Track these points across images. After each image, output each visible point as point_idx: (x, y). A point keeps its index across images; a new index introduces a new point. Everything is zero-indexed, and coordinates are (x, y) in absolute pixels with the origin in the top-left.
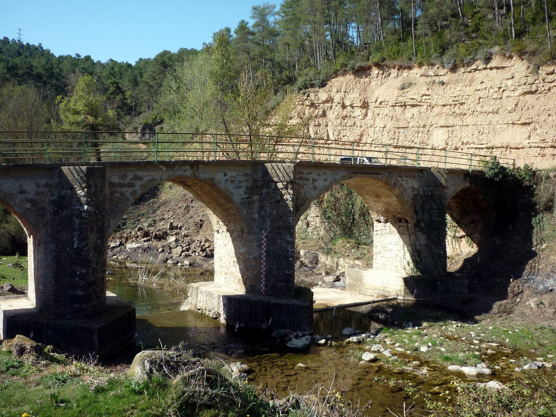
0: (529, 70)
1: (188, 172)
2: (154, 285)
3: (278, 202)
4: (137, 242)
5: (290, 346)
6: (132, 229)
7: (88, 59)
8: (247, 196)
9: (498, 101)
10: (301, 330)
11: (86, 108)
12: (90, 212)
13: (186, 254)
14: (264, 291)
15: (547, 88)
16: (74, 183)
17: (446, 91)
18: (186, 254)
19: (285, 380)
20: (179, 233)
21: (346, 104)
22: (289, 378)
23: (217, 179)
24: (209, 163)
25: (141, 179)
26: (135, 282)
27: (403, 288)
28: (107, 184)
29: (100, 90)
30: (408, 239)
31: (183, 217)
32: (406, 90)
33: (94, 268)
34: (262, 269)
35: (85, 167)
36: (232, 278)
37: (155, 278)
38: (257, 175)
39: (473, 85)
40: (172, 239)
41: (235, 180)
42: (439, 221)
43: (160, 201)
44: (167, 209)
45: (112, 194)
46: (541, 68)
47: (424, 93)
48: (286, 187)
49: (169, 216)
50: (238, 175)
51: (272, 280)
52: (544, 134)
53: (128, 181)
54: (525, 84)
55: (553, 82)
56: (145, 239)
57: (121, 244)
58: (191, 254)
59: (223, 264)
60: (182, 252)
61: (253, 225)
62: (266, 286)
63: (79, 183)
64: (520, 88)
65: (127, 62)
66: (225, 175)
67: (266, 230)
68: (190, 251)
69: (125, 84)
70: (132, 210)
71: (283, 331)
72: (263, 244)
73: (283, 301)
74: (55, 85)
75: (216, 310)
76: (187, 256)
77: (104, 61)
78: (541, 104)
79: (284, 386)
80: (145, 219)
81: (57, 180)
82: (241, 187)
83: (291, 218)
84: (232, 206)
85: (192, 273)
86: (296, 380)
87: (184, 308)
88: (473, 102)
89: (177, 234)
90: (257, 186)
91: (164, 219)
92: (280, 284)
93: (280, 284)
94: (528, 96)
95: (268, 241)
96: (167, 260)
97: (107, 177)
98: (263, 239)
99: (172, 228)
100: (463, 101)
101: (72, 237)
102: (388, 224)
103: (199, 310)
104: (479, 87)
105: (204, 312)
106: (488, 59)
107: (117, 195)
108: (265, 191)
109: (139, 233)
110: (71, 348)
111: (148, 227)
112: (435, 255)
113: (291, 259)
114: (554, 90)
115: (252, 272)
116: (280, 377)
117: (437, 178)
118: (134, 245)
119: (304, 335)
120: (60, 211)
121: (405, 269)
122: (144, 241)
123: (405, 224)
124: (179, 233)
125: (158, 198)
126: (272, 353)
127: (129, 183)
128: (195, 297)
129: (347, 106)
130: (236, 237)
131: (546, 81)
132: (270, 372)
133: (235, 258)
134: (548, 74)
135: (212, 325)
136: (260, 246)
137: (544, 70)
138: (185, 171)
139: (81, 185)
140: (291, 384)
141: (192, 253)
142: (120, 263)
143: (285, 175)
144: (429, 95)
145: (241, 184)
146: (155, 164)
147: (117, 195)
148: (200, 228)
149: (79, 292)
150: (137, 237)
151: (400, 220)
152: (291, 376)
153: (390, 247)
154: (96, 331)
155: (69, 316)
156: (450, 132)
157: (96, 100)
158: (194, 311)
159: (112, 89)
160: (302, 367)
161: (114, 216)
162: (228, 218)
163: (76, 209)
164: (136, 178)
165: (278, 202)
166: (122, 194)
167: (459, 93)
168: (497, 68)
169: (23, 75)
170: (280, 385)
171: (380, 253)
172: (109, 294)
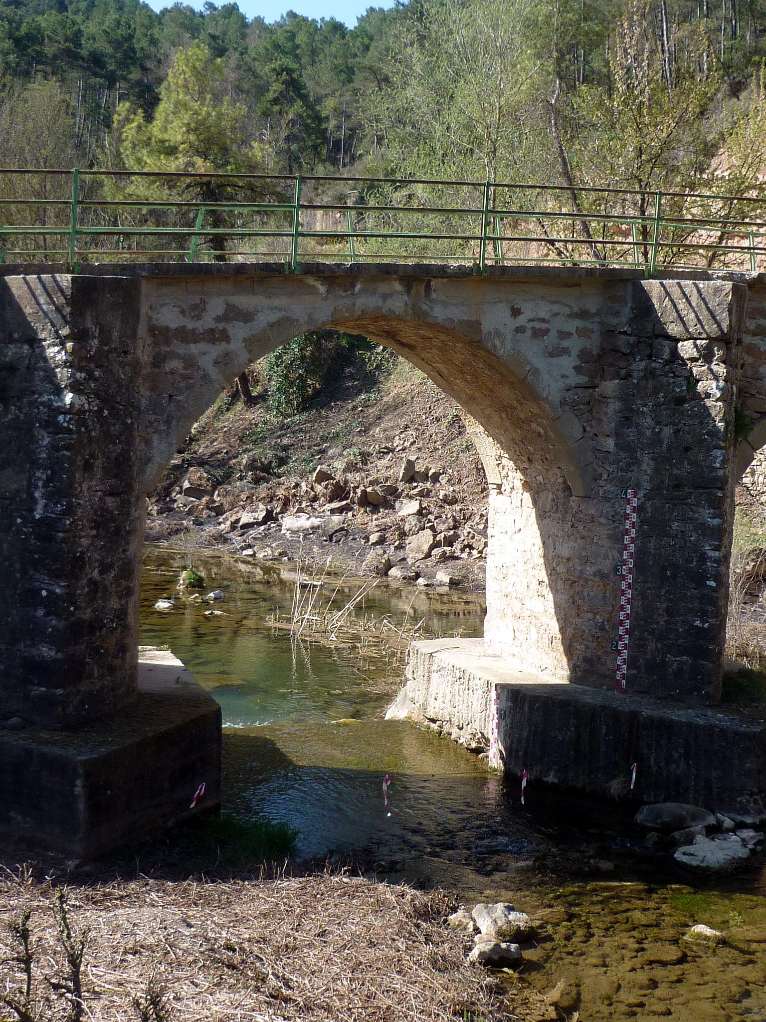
1: (396, 300)
2: (333, 637)
3: (680, 401)
5: (685, 859)
6: (303, 475)
7: (230, 14)
8: (583, 379)
10: (729, 808)
11: (192, 137)
12: (81, 412)
13: (444, 552)
16: (37, 326)
18: (444, 552)
19: (642, 977)
20: (429, 491)
22: (659, 973)
23: (487, 326)
24: (462, 274)
25: (247, 317)
26: (284, 625)
28: (142, 330)
29: (247, 92)
31: (444, 445)
33: (92, 582)
35: (69, 276)
36: (533, 631)
37: (338, 618)
38: (618, 321)
40: (408, 508)
41: (547, 331)
43: (385, 399)
44: (402, 422)
45: (158, 361)
48: (706, 356)
49: (407, 444)
51: (651, 646)
53: (207, 322)
56: (336, 505)
57: (270, 517)
58: (458, 554)
59: (510, 589)
60: (432, 547)
62: (631, 663)
63: (53, 325)
65: (332, 19)
66: (516, 312)
67: (637, 487)
68: (457, 546)
69: (319, 78)
70: (307, 422)
71: (670, 808)
72: (627, 532)
73: (679, 715)
74: (139, 83)
75: (477, 725)
76: (446, 558)
77: (271, 18)
79: (632, 1000)
80: (338, 451)
82: (565, 351)
83: (718, 453)
84: (535, 410)
85: (461, 607)
86: (679, 981)
87: (395, 712)
90: (615, 350)
91: (393, 451)
92: (674, 661)
93: (674, 661)
95: (642, 522)
96: (389, 566)
97: (144, 309)
98: (626, 516)
99: (411, 476)
103: (434, 721)
105: (445, 729)
107: (174, 364)
109: (319, 488)
111: (345, 471)
113: (713, 584)
115: (590, 616)
116: (628, 965)
118: (304, 522)
119: (741, 826)
122: (333, 511)
124: (429, 491)
126: (621, 881)
127: (212, 331)
128: (423, 684)
132: (601, 944)
133: (544, 573)
135: (463, 770)
136: (617, 538)
138: (385, 297)
139: (56, 332)
140: (658, 992)
141: (462, 550)
142: (267, 570)
143: (704, 315)
145: (565, 344)
146: (292, 272)
147: (174, 364)
149: (46, 652)
150: (315, 499)
152: (664, 964)
154: (80, 771)
155: (15, 720)
157: (220, 116)
159: (276, 88)
160: (707, 938)
161: (163, 428)
162: (524, 448)
164: (233, 314)
165: (680, 401)
166: (190, 362)
169: (55, 57)
170: (623, 995)
172: (159, 657)
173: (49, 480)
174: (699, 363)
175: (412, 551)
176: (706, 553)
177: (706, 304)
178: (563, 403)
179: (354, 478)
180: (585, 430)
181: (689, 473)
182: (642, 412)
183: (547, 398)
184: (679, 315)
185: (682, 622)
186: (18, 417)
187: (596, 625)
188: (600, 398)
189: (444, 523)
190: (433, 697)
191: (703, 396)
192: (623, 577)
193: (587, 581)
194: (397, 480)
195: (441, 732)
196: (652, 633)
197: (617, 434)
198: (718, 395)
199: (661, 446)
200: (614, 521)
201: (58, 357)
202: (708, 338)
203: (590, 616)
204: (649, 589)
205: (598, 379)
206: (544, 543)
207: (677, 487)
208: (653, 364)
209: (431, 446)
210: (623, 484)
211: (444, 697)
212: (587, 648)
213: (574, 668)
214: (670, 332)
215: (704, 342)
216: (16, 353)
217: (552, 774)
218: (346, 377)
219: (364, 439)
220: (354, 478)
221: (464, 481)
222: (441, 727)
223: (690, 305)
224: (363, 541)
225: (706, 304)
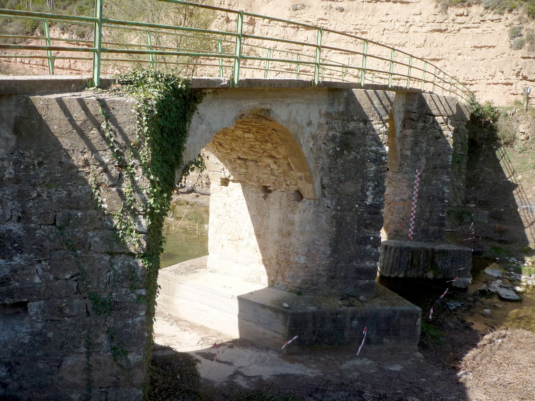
3: (437, 138)
9: (404, 35)
14: (412, 236)
17: (345, 18)
21: (231, 19)
32: (298, 11)
34: (412, 211)
39: (377, 15)
46: (449, 8)
47: (321, 17)
51: (423, 224)
52: (455, 71)
55: (463, 23)
61: (403, 162)
63: (379, 114)
64: (428, 25)
67: (419, 168)
81: (341, 108)
88: (377, 32)
92: (432, 229)
95: (421, 181)
98: (416, 179)
100: (365, 30)
101: (363, 190)
104: (384, 19)
108: (420, 124)
110: (385, 340)
112: (455, 187)
115: (397, 215)
117: (463, 113)
120: (345, 152)
129: (231, 21)
131: (456, 21)
134: (457, 16)
136: (411, 187)
139: (381, 118)
143: (447, 108)
144: (326, 20)
156: (351, 60)
163: (372, 151)
165: (437, 138)
167: (361, 21)
173: (376, 186)
177: (448, 104)
184: (437, 107)
186: (356, 157)
187: (400, 218)
193: (396, 203)
196: (424, 219)
201: (382, 129)
202: (448, 116)
207: (435, 168)
210: (414, 168)
212: (396, 226)
216: (355, 127)
217: (402, 274)
225: (448, 104)
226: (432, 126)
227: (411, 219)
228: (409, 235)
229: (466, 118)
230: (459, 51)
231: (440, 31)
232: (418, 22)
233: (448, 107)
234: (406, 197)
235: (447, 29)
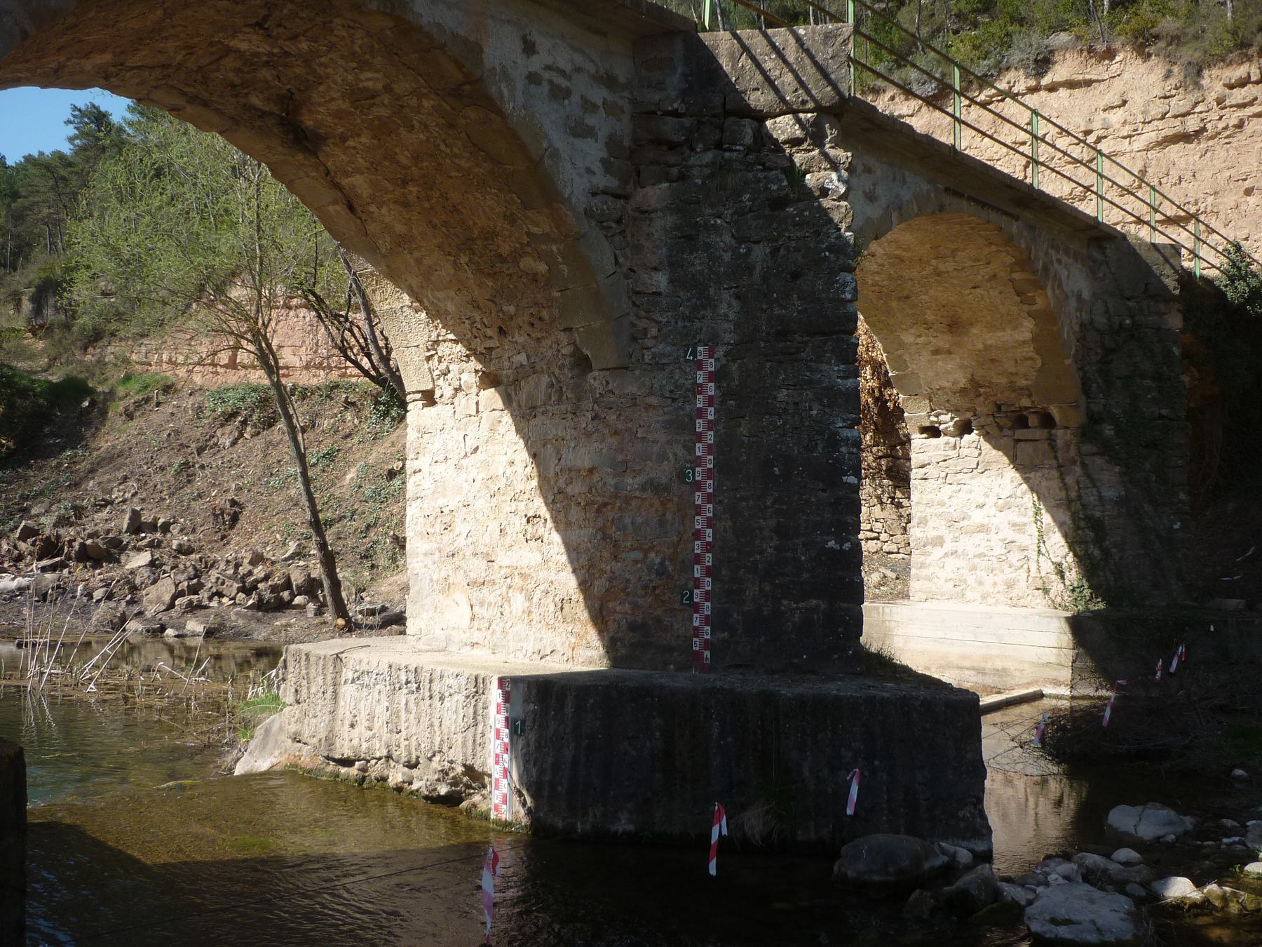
0: (1173, 81)
4: (19, 573)
8: (613, 183)
13: (191, 602)
14: (707, 645)
15: (1234, 121)
18: (191, 602)
20: (160, 542)
27: (1068, 655)
30: (1056, 484)
31: (171, 495)
34: (698, 535)
36: (519, 602)
42: (1161, 417)
44: (120, 475)
46: (1206, 73)
49: (128, 495)
50: (578, 70)
54: (1163, 118)
55: (1251, 103)
56: (45, 562)
58: (205, 602)
59: (461, 542)
60: (174, 597)
61: (642, 324)
64: (1147, 128)
67: (712, 342)
68: (204, 594)
76: (193, 608)
78: (1218, 164)
82: (589, 132)
89: (152, 545)
91: (111, 503)
94: (1174, 150)
95: (726, 395)
96: (123, 619)
98: (697, 389)
99: (137, 527)
102: (974, 436)
103: (347, 762)
106: (1043, 63)
109: (23, 546)
111: (56, 525)
114: (1254, 126)
115: (638, 555)
121: (1046, 591)
122: (44, 569)
123: (1041, 434)
124: (160, 542)
125: (86, 447)
128: (322, 705)
130: (541, 396)
131: (1227, 103)
134: (1231, 87)
135: (430, 835)
136: (682, 426)
137: (1215, 81)
141: (210, 599)
145: (591, 120)
148: (232, 527)
150: (20, 558)
151: (1021, 421)
153: (978, 517)
158: (319, 771)
165: (779, 203)
168: (1071, 85)
171: (939, 541)
174: (805, 146)
175: (150, 602)
176: (838, 433)
177: (812, 57)
178: (588, 213)
179: (67, 533)
180: (617, 263)
181: (799, 312)
182: (715, 226)
183: (569, 199)
185: (804, 545)
188: (637, 214)
189: (183, 572)
190: (347, 723)
191: (817, 194)
192: (698, 486)
193: (627, 500)
194: (120, 532)
195: (364, 778)
197: (671, 265)
198: (842, 190)
199: (751, 274)
200: (674, 400)
202: (819, 108)
203: (638, 555)
204: (742, 499)
205: (632, 184)
206: (534, 456)
208: (727, 155)
209: (158, 497)
211: (371, 718)
212: (635, 606)
213: (612, 646)
214: (752, 103)
215: (809, 115)
217: (624, 817)
218: (46, 436)
219: (75, 493)
220: (67, 533)
221: (200, 529)
222: (364, 770)
223: (785, 61)
224: (85, 599)
225: (812, 57)
226: (751, 157)
227: (698, 571)
228: (697, 644)
229: (1166, 287)
230: (1247, 184)
231: (1185, 138)
232: (1117, 126)
233: (811, 70)
234: (663, 472)
235: (1204, 129)
